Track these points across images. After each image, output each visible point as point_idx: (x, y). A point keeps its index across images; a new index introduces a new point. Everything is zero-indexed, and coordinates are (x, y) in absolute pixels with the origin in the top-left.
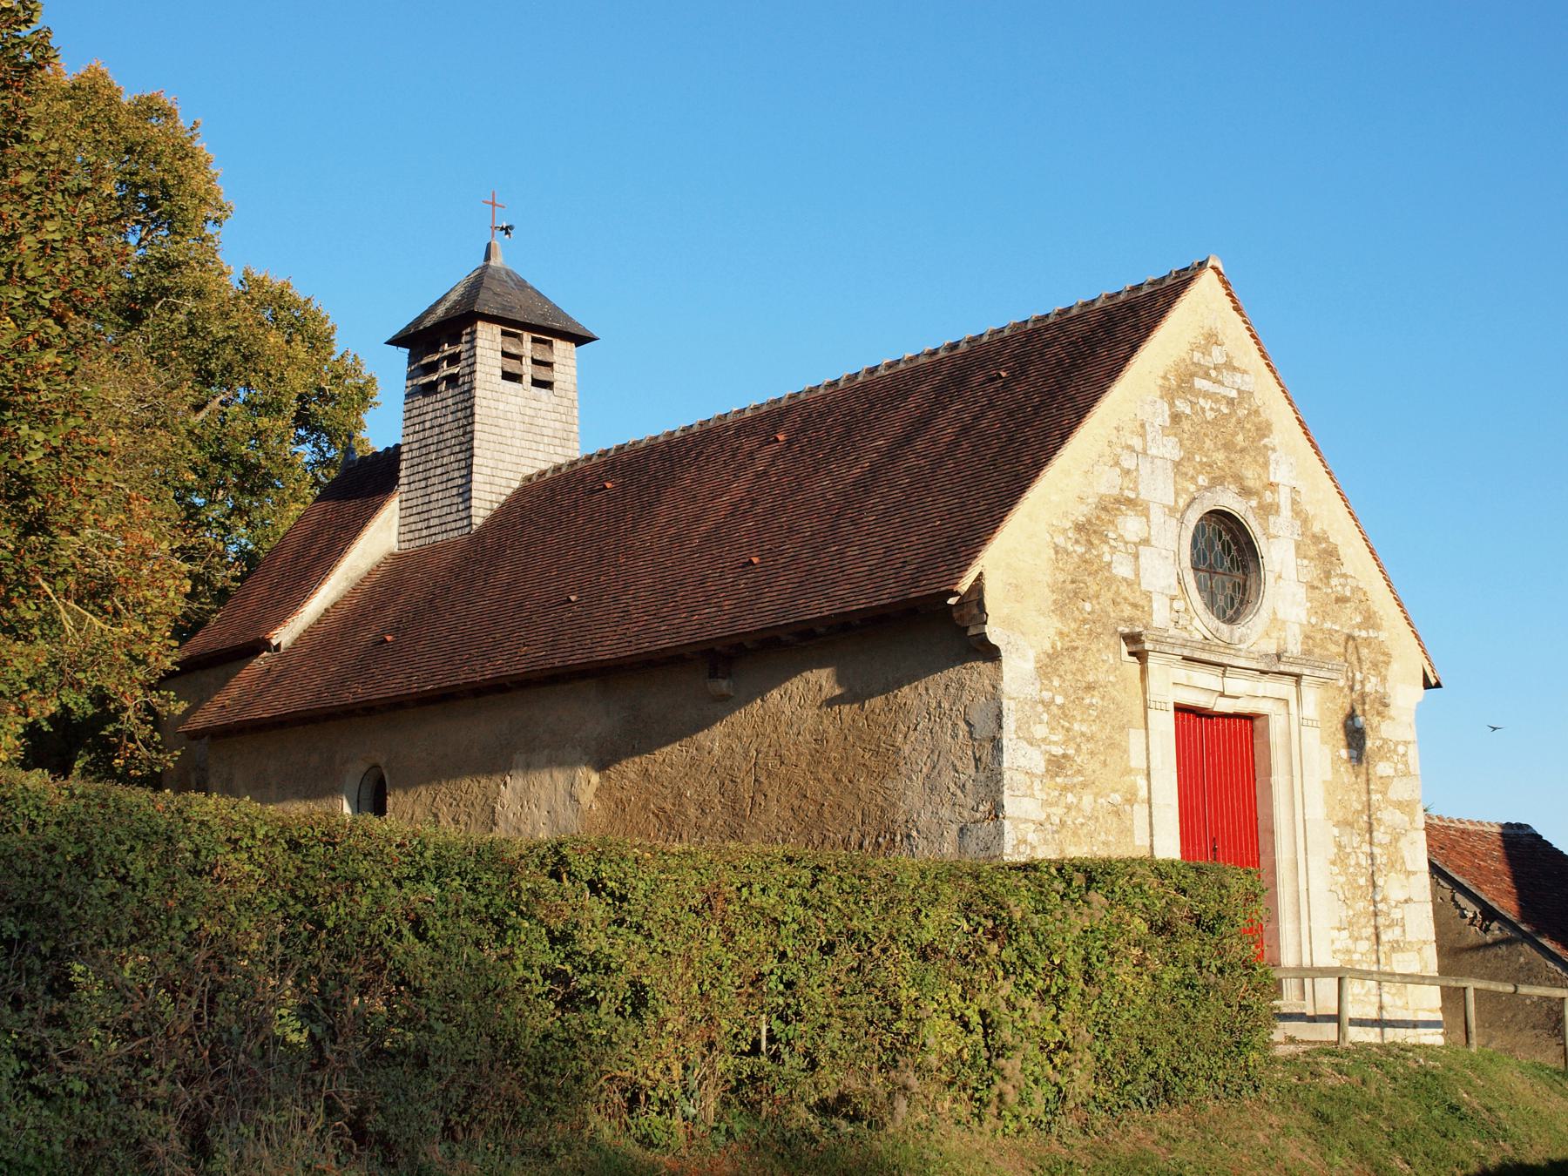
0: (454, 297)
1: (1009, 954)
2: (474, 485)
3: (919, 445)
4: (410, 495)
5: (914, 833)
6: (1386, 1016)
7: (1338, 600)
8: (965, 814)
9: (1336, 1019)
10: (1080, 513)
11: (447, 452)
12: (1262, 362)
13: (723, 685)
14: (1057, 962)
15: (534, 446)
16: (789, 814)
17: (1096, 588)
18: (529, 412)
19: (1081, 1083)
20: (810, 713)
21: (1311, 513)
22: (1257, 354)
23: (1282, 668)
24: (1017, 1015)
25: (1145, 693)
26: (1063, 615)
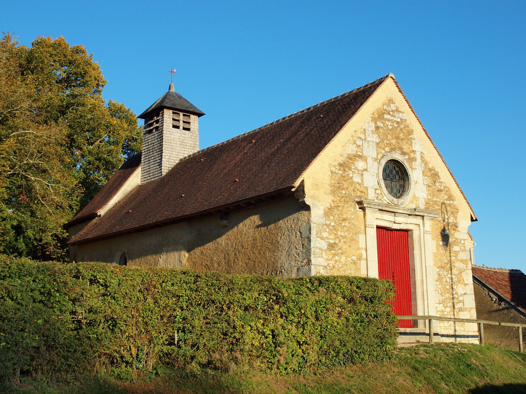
0: (158, 102)
1: (283, 309)
2: (163, 162)
3: (292, 140)
4: (144, 166)
5: (283, 271)
6: (457, 334)
7: (438, 191)
8: (299, 264)
9: (429, 335)
10: (341, 160)
11: (155, 152)
12: (410, 110)
13: (225, 222)
14: (303, 312)
15: (184, 149)
16: (245, 265)
17: (347, 185)
18: (181, 138)
19: (313, 357)
20: (252, 231)
21: (428, 161)
22: (408, 107)
23: (416, 213)
24: (286, 331)
25: (365, 222)
26: (334, 195)
